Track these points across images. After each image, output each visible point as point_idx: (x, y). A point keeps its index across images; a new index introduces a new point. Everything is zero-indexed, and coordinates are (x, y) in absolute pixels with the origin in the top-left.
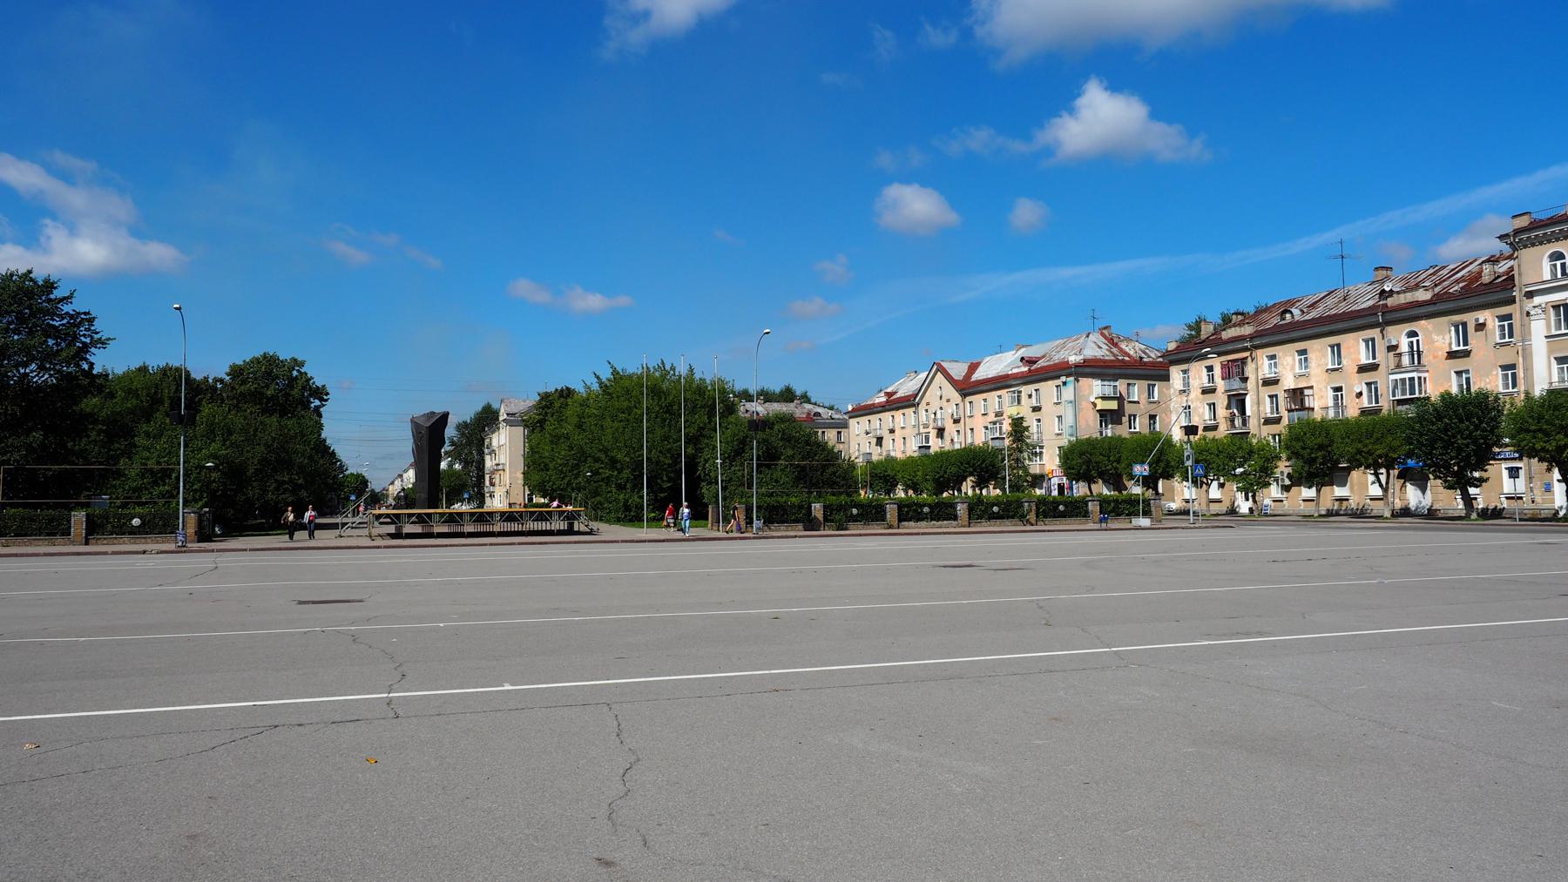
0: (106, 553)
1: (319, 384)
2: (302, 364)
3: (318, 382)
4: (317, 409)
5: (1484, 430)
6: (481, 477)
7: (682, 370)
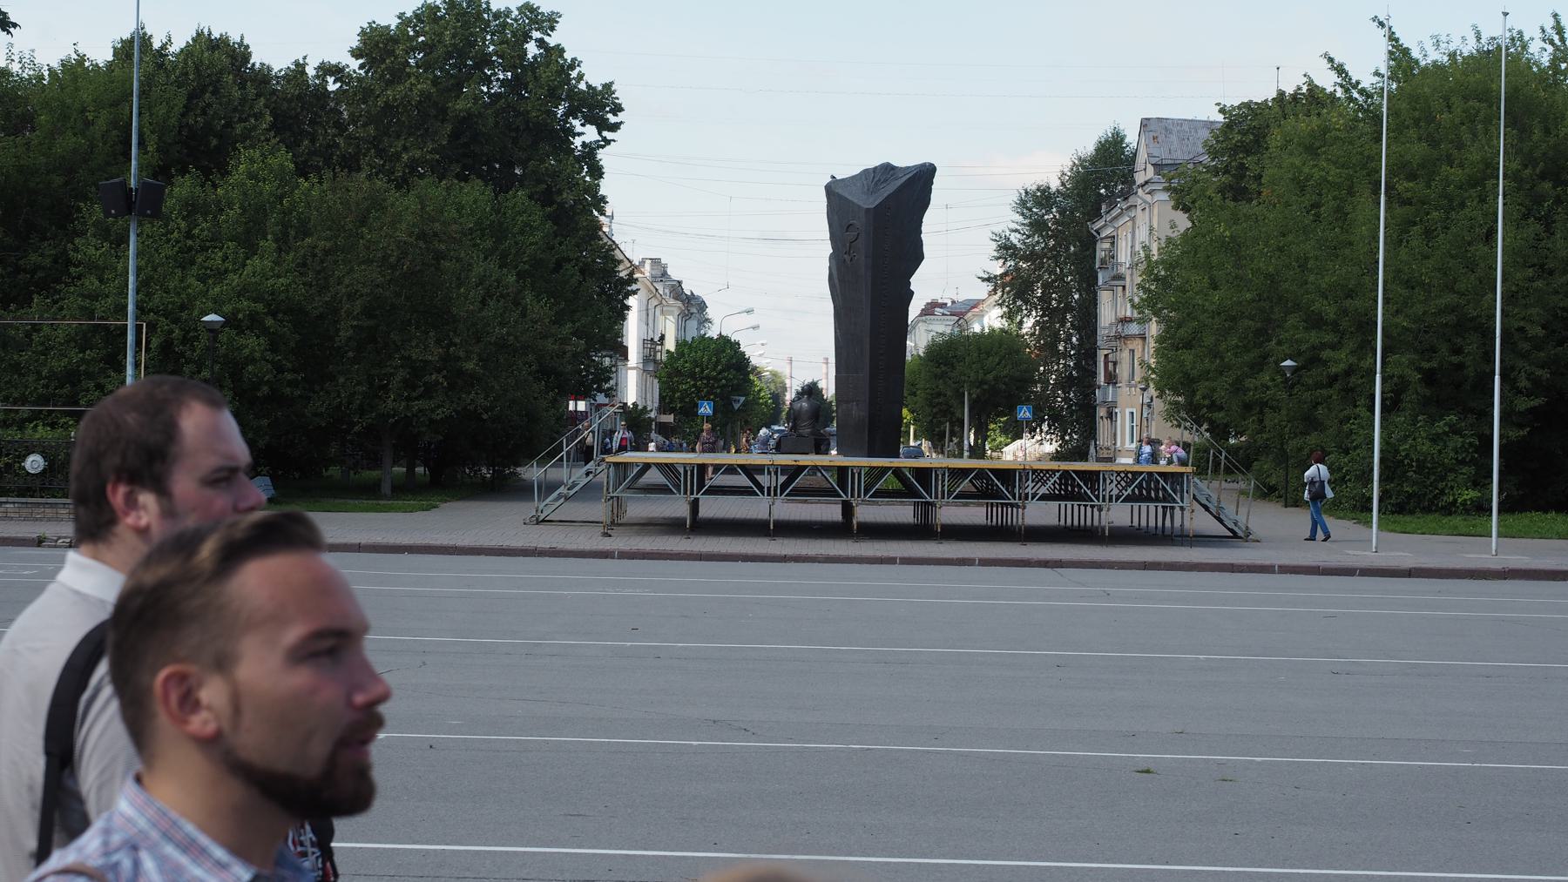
0: (890, 561)
1: (597, 83)
2: (550, 22)
3: (593, 75)
4: (590, 151)
5: (708, 378)
6: (1087, 353)
7: (1368, 66)
